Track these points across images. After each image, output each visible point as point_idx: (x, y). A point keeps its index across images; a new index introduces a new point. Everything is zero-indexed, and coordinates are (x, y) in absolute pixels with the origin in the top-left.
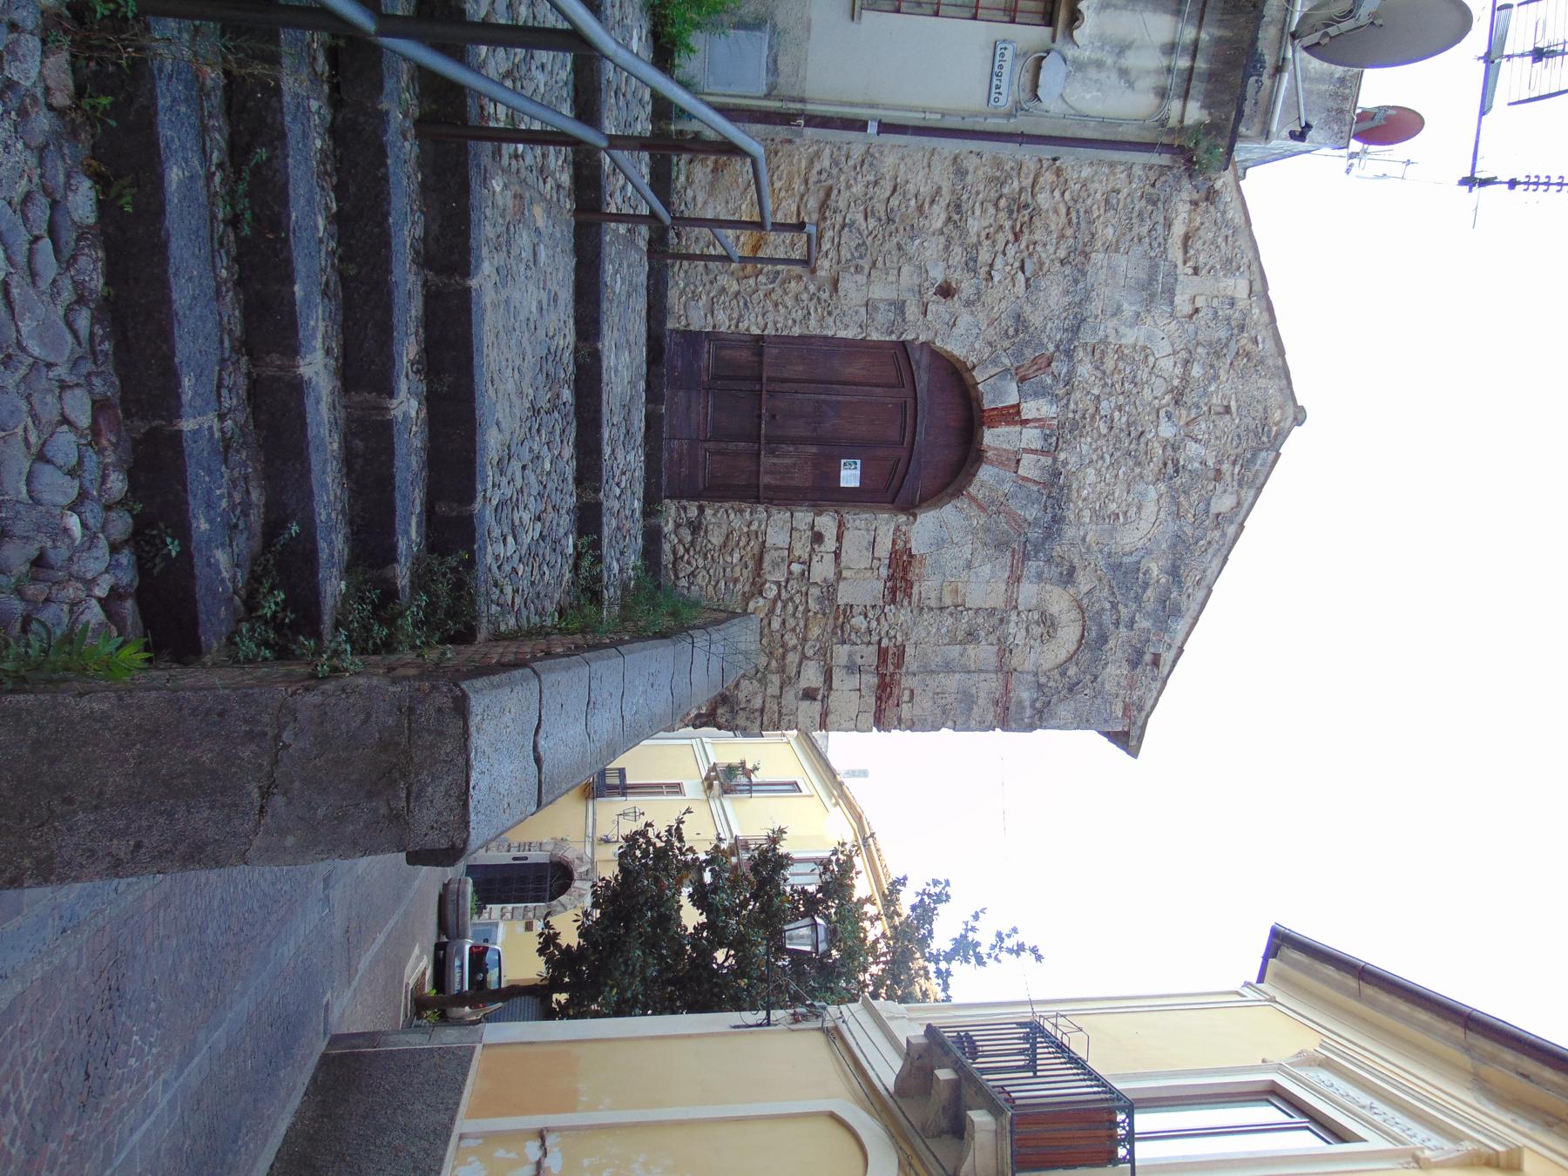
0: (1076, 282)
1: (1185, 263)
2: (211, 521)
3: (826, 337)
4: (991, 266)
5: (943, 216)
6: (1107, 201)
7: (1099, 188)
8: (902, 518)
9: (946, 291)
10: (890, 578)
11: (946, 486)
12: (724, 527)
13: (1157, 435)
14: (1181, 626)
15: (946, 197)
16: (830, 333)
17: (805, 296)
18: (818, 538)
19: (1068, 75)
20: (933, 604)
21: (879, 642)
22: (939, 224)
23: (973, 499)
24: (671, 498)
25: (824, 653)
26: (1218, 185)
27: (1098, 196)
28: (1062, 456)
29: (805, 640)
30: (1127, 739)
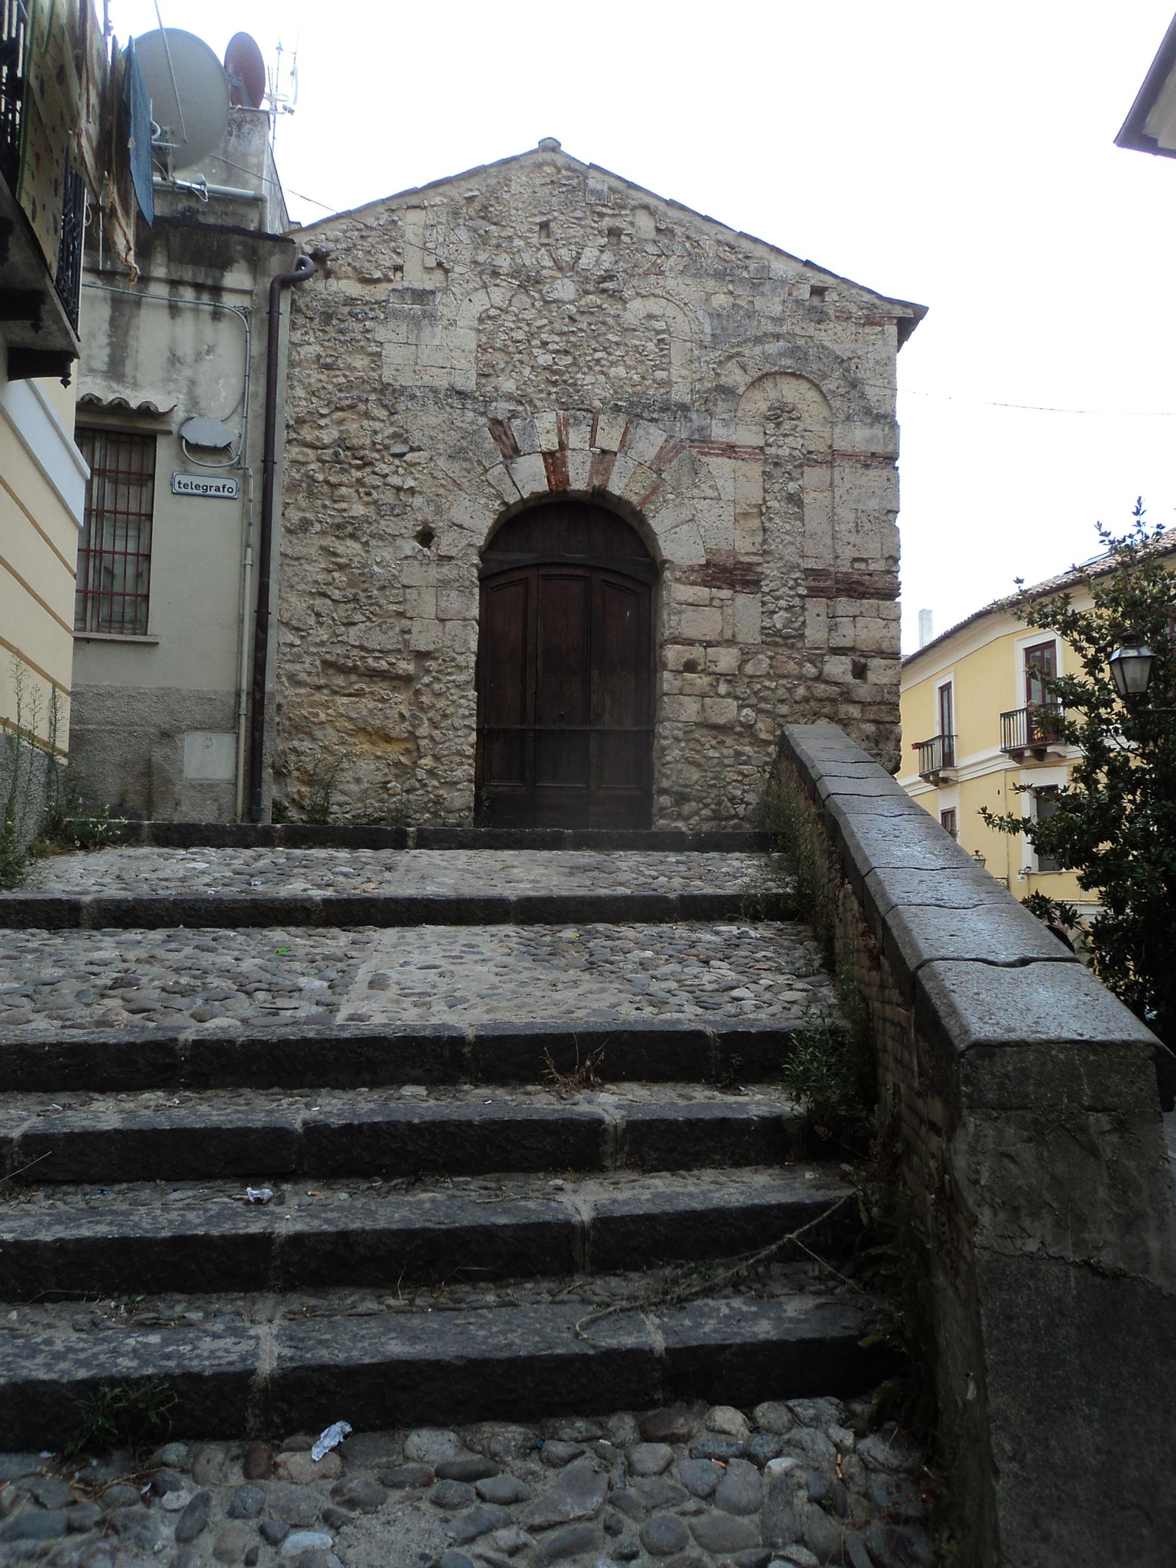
0: (413, 397)
1: (390, 281)
2: (756, 1317)
3: (477, 663)
4: (399, 489)
5: (350, 542)
6: (328, 367)
7: (316, 377)
8: (667, 574)
9: (426, 537)
10: (732, 586)
11: (632, 531)
12: (680, 766)
13: (571, 302)
14: (779, 268)
15: (328, 541)
16: (473, 658)
17: (436, 686)
18: (690, 666)
19: (201, 415)
20: (759, 539)
21: (802, 597)
22: (357, 546)
23: (646, 500)
24: (650, 824)
25: (816, 659)
26: (309, 249)
27: (323, 377)
28: (597, 404)
29: (800, 677)
30: (906, 319)
